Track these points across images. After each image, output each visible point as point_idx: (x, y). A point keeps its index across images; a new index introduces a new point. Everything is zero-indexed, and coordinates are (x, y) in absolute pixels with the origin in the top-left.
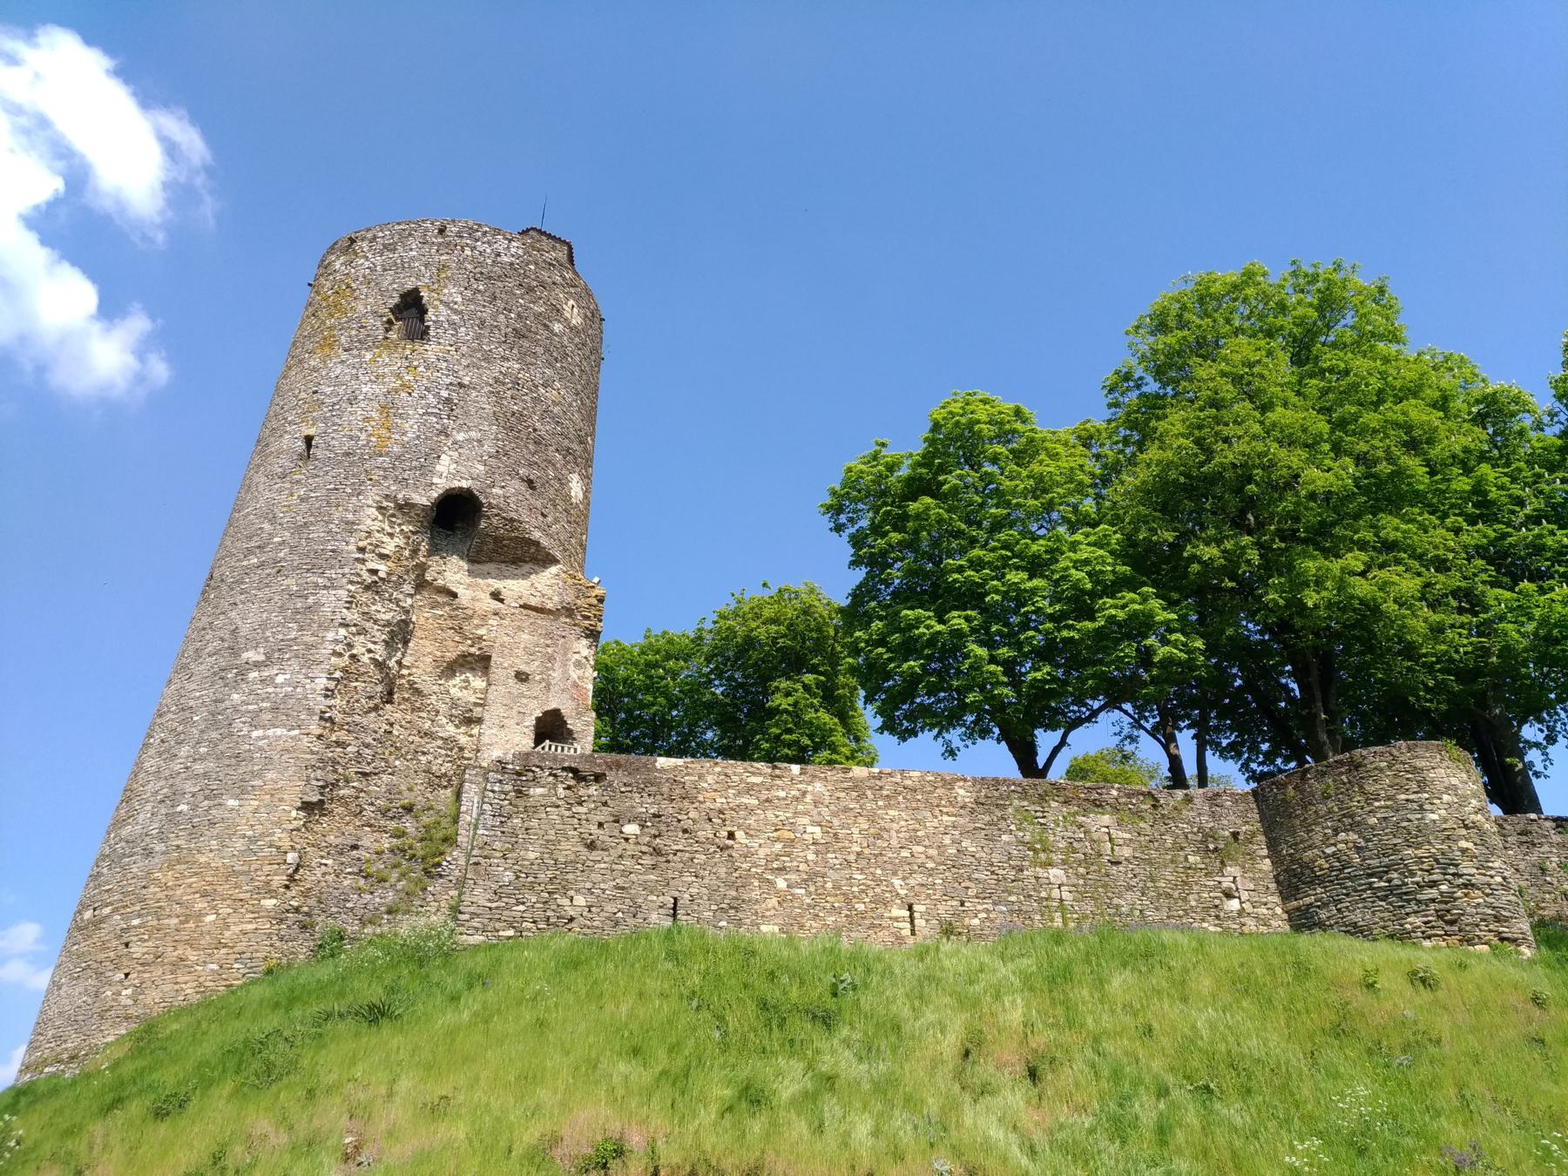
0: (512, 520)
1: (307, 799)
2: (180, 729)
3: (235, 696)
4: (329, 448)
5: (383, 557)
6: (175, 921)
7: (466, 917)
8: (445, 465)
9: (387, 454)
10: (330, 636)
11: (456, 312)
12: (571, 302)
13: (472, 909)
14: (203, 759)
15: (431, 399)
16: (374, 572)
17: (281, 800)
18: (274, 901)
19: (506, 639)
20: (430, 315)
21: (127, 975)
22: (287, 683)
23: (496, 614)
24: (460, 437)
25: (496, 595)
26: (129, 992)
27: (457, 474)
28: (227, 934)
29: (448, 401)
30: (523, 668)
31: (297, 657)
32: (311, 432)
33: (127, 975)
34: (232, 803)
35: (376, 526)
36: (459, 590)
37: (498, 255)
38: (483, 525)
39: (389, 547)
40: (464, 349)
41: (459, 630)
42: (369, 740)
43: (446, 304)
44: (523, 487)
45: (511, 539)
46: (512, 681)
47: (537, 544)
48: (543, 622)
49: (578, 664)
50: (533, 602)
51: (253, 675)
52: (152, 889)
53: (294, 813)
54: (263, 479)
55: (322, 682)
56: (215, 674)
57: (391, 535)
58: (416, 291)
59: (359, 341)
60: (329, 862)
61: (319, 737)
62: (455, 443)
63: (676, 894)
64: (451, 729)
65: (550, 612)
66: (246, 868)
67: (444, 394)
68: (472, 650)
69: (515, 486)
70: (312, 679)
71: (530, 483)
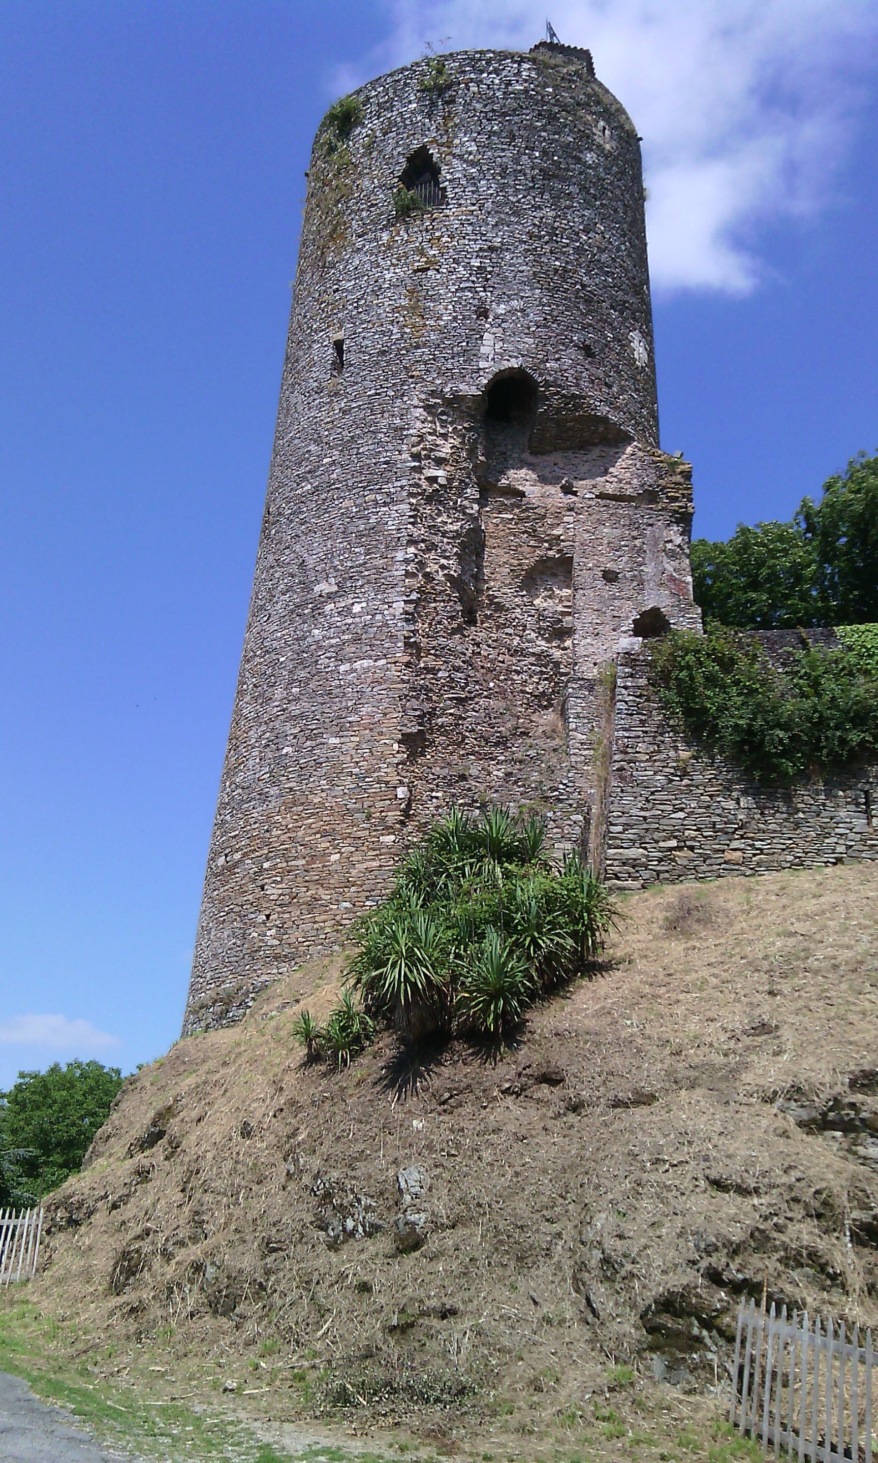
3: (316, 632)
7: (620, 829)
8: (488, 345)
9: (424, 345)
10: (400, 556)
11: (473, 164)
12: (602, 123)
14: (297, 699)
16: (432, 480)
17: (381, 733)
18: (392, 837)
19: (586, 536)
21: (268, 916)
22: (364, 612)
24: (501, 309)
27: (502, 355)
28: (354, 872)
31: (369, 582)
32: (340, 336)
33: (268, 916)
34: (334, 741)
39: (445, 450)
40: (489, 205)
41: (533, 533)
42: (458, 663)
43: (460, 157)
45: (575, 419)
46: (600, 584)
47: (605, 420)
48: (623, 510)
51: (330, 607)
56: (292, 612)
57: (444, 436)
58: (424, 149)
60: (440, 794)
65: (630, 499)
66: (358, 806)
67: (476, 263)
71: (587, 351)
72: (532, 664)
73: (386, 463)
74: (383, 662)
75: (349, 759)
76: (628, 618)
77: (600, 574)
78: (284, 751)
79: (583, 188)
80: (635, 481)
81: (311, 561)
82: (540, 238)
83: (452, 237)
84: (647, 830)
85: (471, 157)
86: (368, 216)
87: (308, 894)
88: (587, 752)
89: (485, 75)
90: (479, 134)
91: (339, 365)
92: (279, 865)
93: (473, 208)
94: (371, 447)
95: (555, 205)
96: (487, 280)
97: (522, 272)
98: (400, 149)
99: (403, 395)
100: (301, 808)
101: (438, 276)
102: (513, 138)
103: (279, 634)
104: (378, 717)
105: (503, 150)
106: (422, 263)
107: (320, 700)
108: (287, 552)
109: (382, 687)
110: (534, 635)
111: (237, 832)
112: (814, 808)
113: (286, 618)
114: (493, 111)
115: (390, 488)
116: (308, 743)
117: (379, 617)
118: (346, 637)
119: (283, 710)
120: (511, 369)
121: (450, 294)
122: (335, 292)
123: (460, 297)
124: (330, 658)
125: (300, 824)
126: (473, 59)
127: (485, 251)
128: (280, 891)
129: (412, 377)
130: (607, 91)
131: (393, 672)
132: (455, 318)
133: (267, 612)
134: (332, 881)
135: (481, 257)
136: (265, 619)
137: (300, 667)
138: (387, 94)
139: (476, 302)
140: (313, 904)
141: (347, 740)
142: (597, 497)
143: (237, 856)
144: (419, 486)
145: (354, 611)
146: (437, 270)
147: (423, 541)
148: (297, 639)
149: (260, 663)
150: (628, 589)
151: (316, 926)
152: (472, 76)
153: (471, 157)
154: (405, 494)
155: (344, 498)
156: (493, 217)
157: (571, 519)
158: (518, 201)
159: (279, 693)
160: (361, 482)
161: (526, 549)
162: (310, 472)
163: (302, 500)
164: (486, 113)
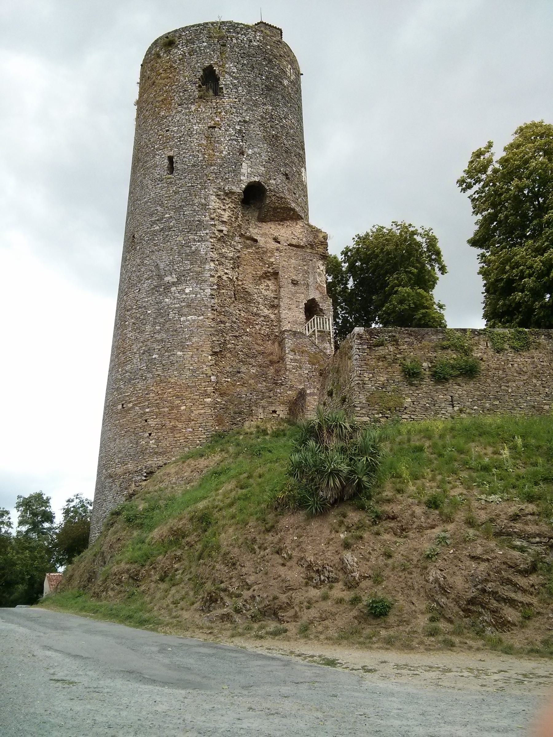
0: (282, 198)
1: (214, 350)
2: (142, 317)
3: (167, 300)
4: (183, 163)
5: (223, 222)
6: (166, 409)
7: (359, 409)
8: (245, 169)
9: (215, 165)
10: (207, 267)
11: (235, 78)
12: (289, 66)
13: (360, 405)
14: (159, 332)
15: (232, 131)
16: (221, 231)
17: (202, 351)
18: (210, 399)
19: (284, 263)
20: (222, 82)
21: (150, 434)
22: (191, 292)
23: (277, 250)
24: (250, 152)
25: (276, 240)
26: (153, 441)
27: (250, 175)
28: (193, 415)
29: (240, 131)
30: (294, 277)
31: (193, 278)
32: (171, 154)
33: (150, 434)
34: (179, 353)
35: (217, 205)
36: (258, 238)
37: (251, 41)
38: (268, 201)
39: (226, 216)
40: (243, 100)
41: (262, 260)
42: (234, 320)
43: (229, 74)
44: (284, 178)
45: (281, 208)
46: (290, 286)
47: (293, 210)
48: (300, 252)
49: (320, 275)
50: (294, 242)
51: (173, 289)
52: (151, 395)
53: (210, 357)
54: (150, 182)
55: (208, 291)
56: (153, 289)
57: (224, 210)
58: (211, 67)
59: (186, 99)
60: (229, 380)
61: (213, 319)
62: (248, 156)
63: (452, 394)
64: (266, 312)
65: (302, 247)
66: (194, 384)
67: (238, 127)
68: (269, 270)
69: (280, 178)
70: (204, 290)
72: (263, 321)
73: (198, 221)
74: (202, 317)
75: (188, 362)
76: (302, 302)
77: (290, 281)
78: (154, 357)
79: (283, 97)
80: (304, 239)
81: (162, 266)
82: (266, 119)
83: (226, 113)
84: (370, 410)
85: (234, 75)
86: (183, 96)
87: (171, 424)
88: (293, 364)
89: (240, 35)
90: (237, 63)
91: (171, 168)
92: (155, 411)
93: (236, 100)
94: (191, 212)
95: (272, 104)
96: (243, 137)
97: (258, 135)
98: (199, 64)
99: (205, 188)
100: (165, 384)
101: (220, 132)
102: (253, 68)
103: (146, 299)
104: (201, 343)
105: (249, 73)
106: (212, 123)
107: (171, 333)
108: (148, 259)
109: (202, 329)
110: (262, 307)
111: (129, 394)
112: (433, 402)
113: (150, 292)
114: (244, 53)
115: (202, 233)
116: (167, 353)
117: (198, 296)
118: (183, 304)
119: (152, 337)
120: (255, 181)
121: (226, 141)
122: (167, 131)
123: (231, 144)
124: (175, 314)
125: (164, 391)
126: (234, 26)
127: (242, 122)
128: (156, 423)
129: (209, 180)
130: (291, 51)
131: (208, 323)
132: (229, 153)
133: (138, 288)
134: (182, 419)
135: (240, 125)
136: (138, 291)
137: (160, 317)
138: (191, 35)
139: (238, 147)
140: (173, 429)
141: (187, 353)
142: (288, 245)
143: (130, 405)
144: (214, 234)
145: (186, 292)
146: (220, 128)
147: (217, 260)
148: (157, 303)
149: (136, 313)
150: (302, 289)
151: (175, 439)
152: (234, 34)
153: (234, 75)
154: (208, 237)
155: (178, 236)
156: (245, 106)
157: (278, 255)
158: (256, 100)
159: (148, 328)
160: (186, 229)
161: (258, 267)
162: (158, 220)
163: (155, 233)
164: (241, 54)
